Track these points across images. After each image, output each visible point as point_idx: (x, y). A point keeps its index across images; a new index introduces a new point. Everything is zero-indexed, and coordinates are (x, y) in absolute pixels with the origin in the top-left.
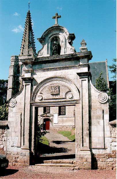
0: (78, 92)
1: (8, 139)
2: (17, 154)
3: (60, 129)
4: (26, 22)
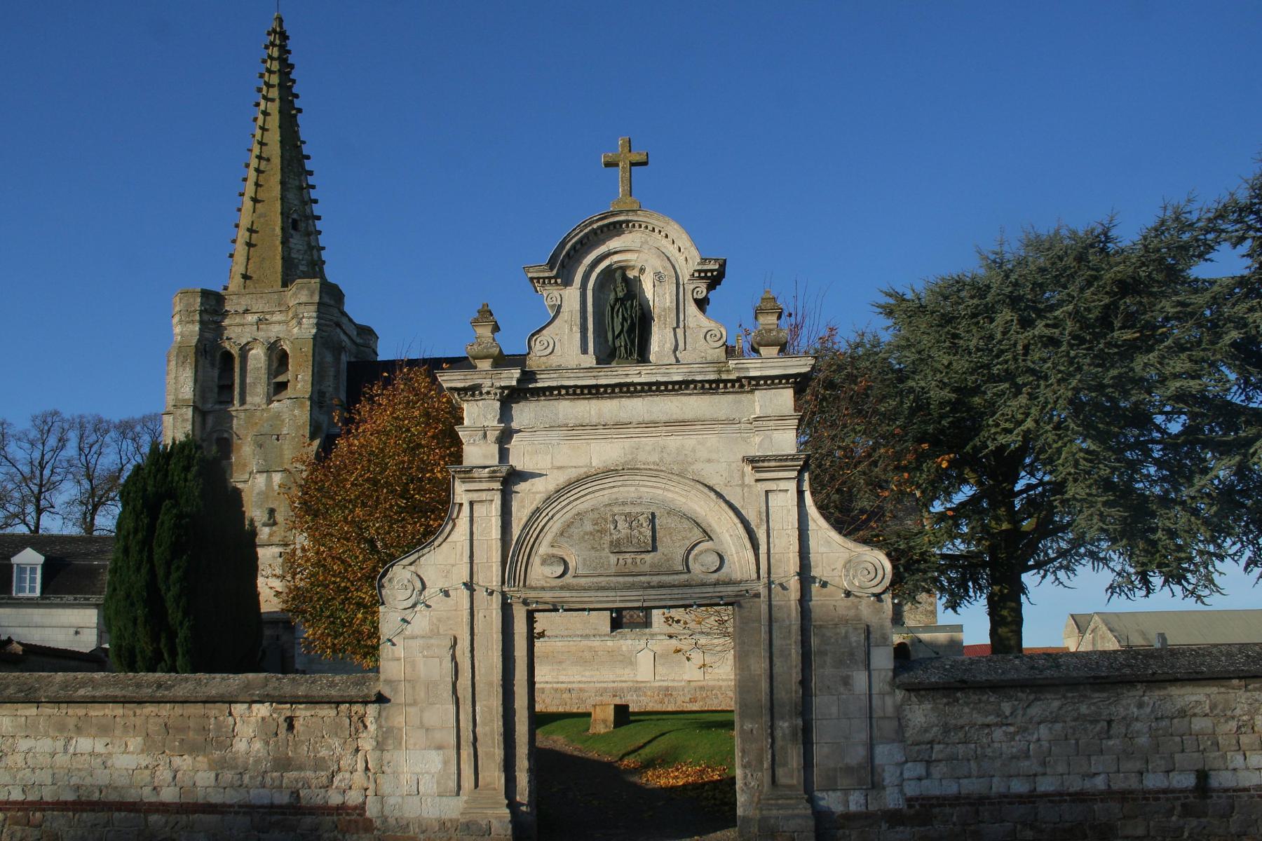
0: (748, 545)
1: (385, 763)
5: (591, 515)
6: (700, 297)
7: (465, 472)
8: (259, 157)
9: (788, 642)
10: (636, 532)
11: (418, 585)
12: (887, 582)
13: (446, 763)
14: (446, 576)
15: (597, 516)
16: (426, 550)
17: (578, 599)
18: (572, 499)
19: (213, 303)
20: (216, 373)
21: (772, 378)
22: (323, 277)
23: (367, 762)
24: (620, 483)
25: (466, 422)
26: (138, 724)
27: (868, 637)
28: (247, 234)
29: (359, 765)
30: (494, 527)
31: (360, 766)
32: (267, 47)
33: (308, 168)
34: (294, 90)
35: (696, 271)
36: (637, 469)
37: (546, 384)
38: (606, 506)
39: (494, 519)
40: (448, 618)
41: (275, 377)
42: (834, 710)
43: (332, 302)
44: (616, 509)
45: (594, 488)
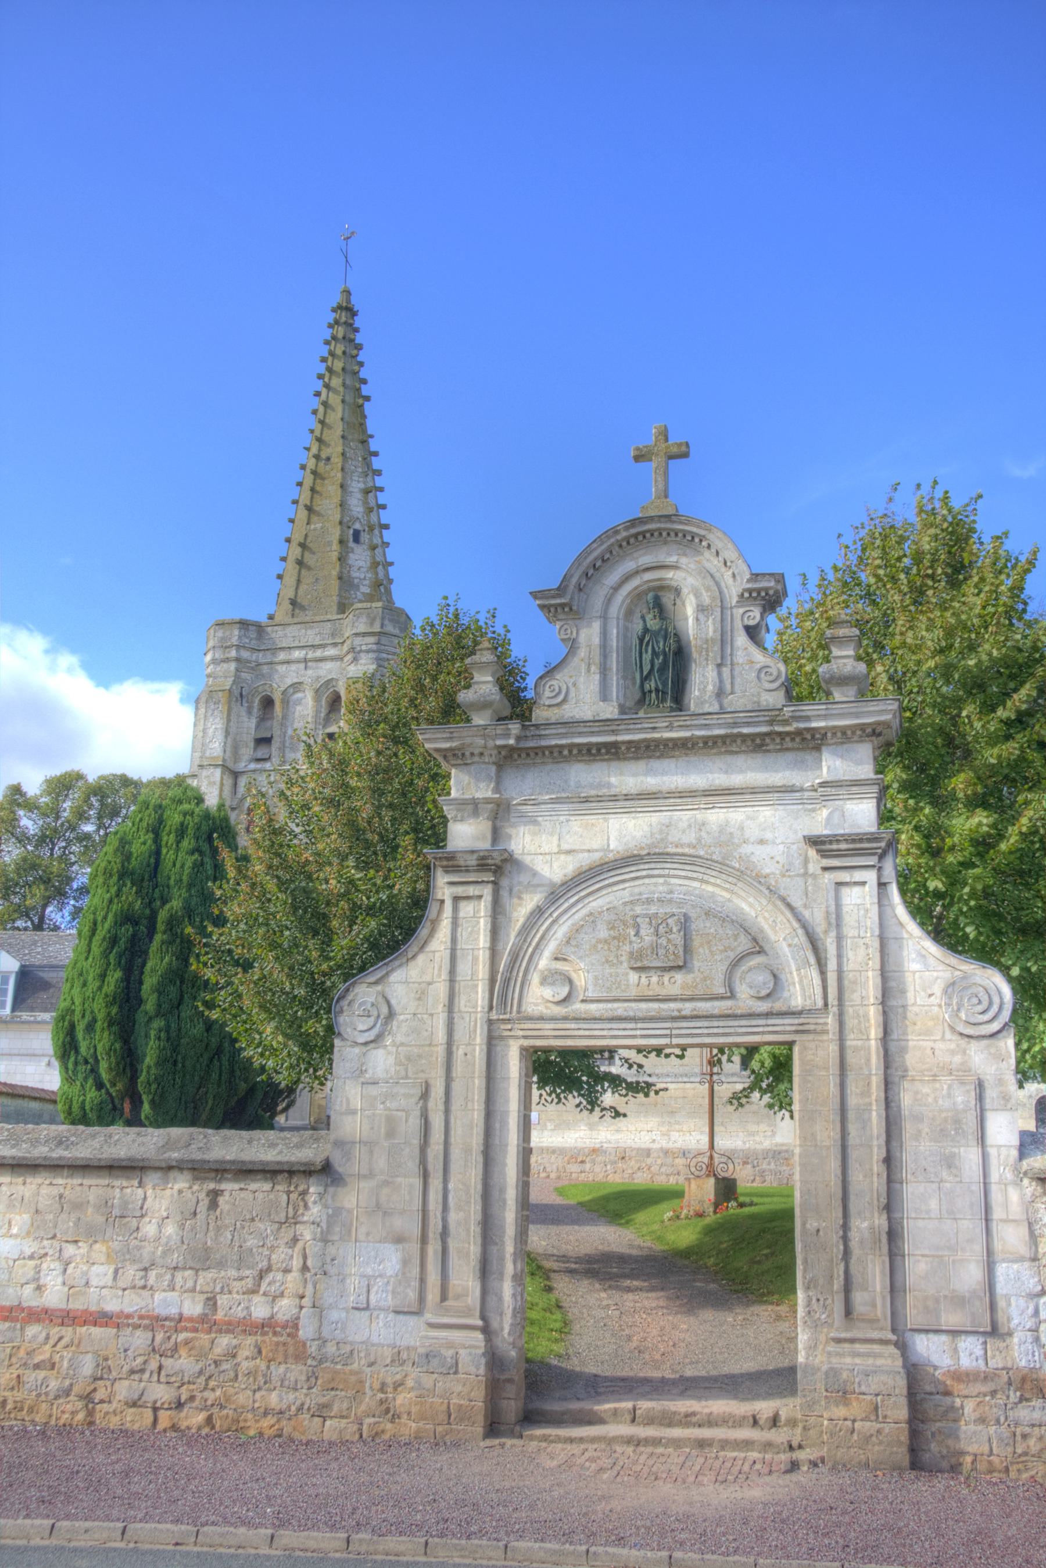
0: (812, 960)
2: (398, 1359)
3: (574, 1168)
4: (320, 377)
5: (606, 916)
6: (752, 623)
7: (448, 859)
8: (317, 457)
9: (867, 1100)
10: (663, 941)
11: (385, 1010)
12: (1006, 1014)
13: (405, 1262)
14: (419, 999)
15: (613, 917)
16: (397, 963)
17: (587, 1033)
18: (582, 894)
19: (253, 635)
20: (254, 722)
21: (843, 730)
22: (390, 601)
23: (305, 1257)
24: (644, 873)
25: (454, 794)
26: (27, 1195)
27: (980, 1098)
28: (299, 550)
29: (295, 1263)
30: (482, 931)
31: (296, 1263)
32: (331, 326)
33: (375, 466)
34: (362, 375)
35: (745, 590)
36: (667, 854)
37: (553, 742)
38: (625, 904)
39: (482, 921)
40: (420, 1056)
41: (324, 727)
42: (934, 1204)
43: (397, 631)
44: (638, 910)
45: (611, 880)
